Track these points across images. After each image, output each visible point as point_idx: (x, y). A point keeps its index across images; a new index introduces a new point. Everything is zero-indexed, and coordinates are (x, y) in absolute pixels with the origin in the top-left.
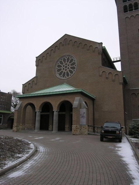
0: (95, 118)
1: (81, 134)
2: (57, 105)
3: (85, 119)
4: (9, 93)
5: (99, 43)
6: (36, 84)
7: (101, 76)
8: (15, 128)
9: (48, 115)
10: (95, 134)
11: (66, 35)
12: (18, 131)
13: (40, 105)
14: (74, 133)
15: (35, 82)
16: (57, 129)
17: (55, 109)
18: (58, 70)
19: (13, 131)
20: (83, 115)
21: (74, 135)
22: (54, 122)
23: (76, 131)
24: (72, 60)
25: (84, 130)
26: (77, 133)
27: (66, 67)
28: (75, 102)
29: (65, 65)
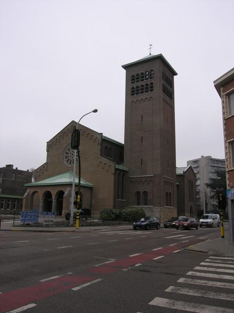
2: (55, 194)
4: (28, 170)
6: (46, 170)
13: (42, 194)
15: (46, 167)
18: (67, 157)
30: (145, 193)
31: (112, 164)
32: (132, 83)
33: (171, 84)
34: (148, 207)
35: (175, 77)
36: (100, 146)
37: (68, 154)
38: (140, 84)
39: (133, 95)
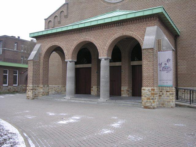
0: (179, 72)
1: (162, 105)
2: (106, 48)
8: (30, 93)
9: (90, 68)
12: (35, 97)
13: (73, 48)
14: (148, 104)
16: (109, 94)
17: (104, 55)
19: (28, 98)
20: (166, 64)
21: (146, 107)
22: (102, 80)
23: (152, 101)
25: (168, 96)
26: (155, 105)
28: (146, 38)
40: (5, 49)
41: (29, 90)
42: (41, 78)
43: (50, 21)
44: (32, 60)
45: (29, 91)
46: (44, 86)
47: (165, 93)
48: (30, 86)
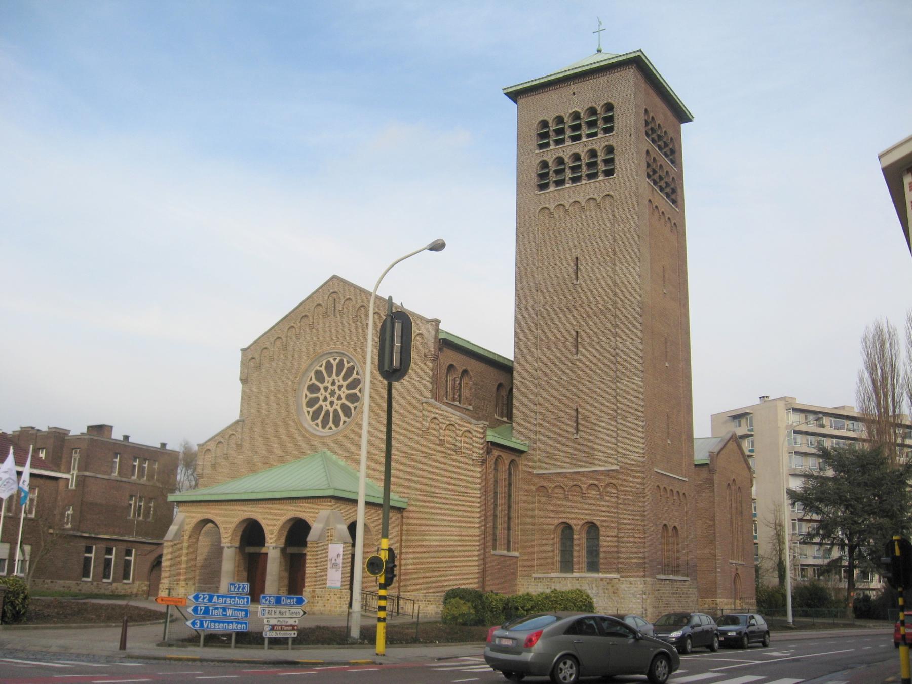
2: (275, 532)
3: (340, 571)
5: (428, 321)
6: (239, 447)
7: (425, 432)
10: (293, 616)
11: (334, 277)
15: (238, 436)
20: (336, 560)
24: (351, 370)
27: (333, 393)
29: (329, 385)
30: (592, 529)
31: (476, 427)
32: (541, 147)
33: (673, 152)
34: (602, 579)
35: (684, 127)
36: (430, 365)
37: (349, 387)
38: (567, 150)
39: (543, 187)
40: (87, 473)
41: (163, 588)
42: (183, 570)
43: (209, 450)
44: (171, 541)
45: (162, 591)
46: (187, 584)
47: (332, 596)
48: (164, 583)
